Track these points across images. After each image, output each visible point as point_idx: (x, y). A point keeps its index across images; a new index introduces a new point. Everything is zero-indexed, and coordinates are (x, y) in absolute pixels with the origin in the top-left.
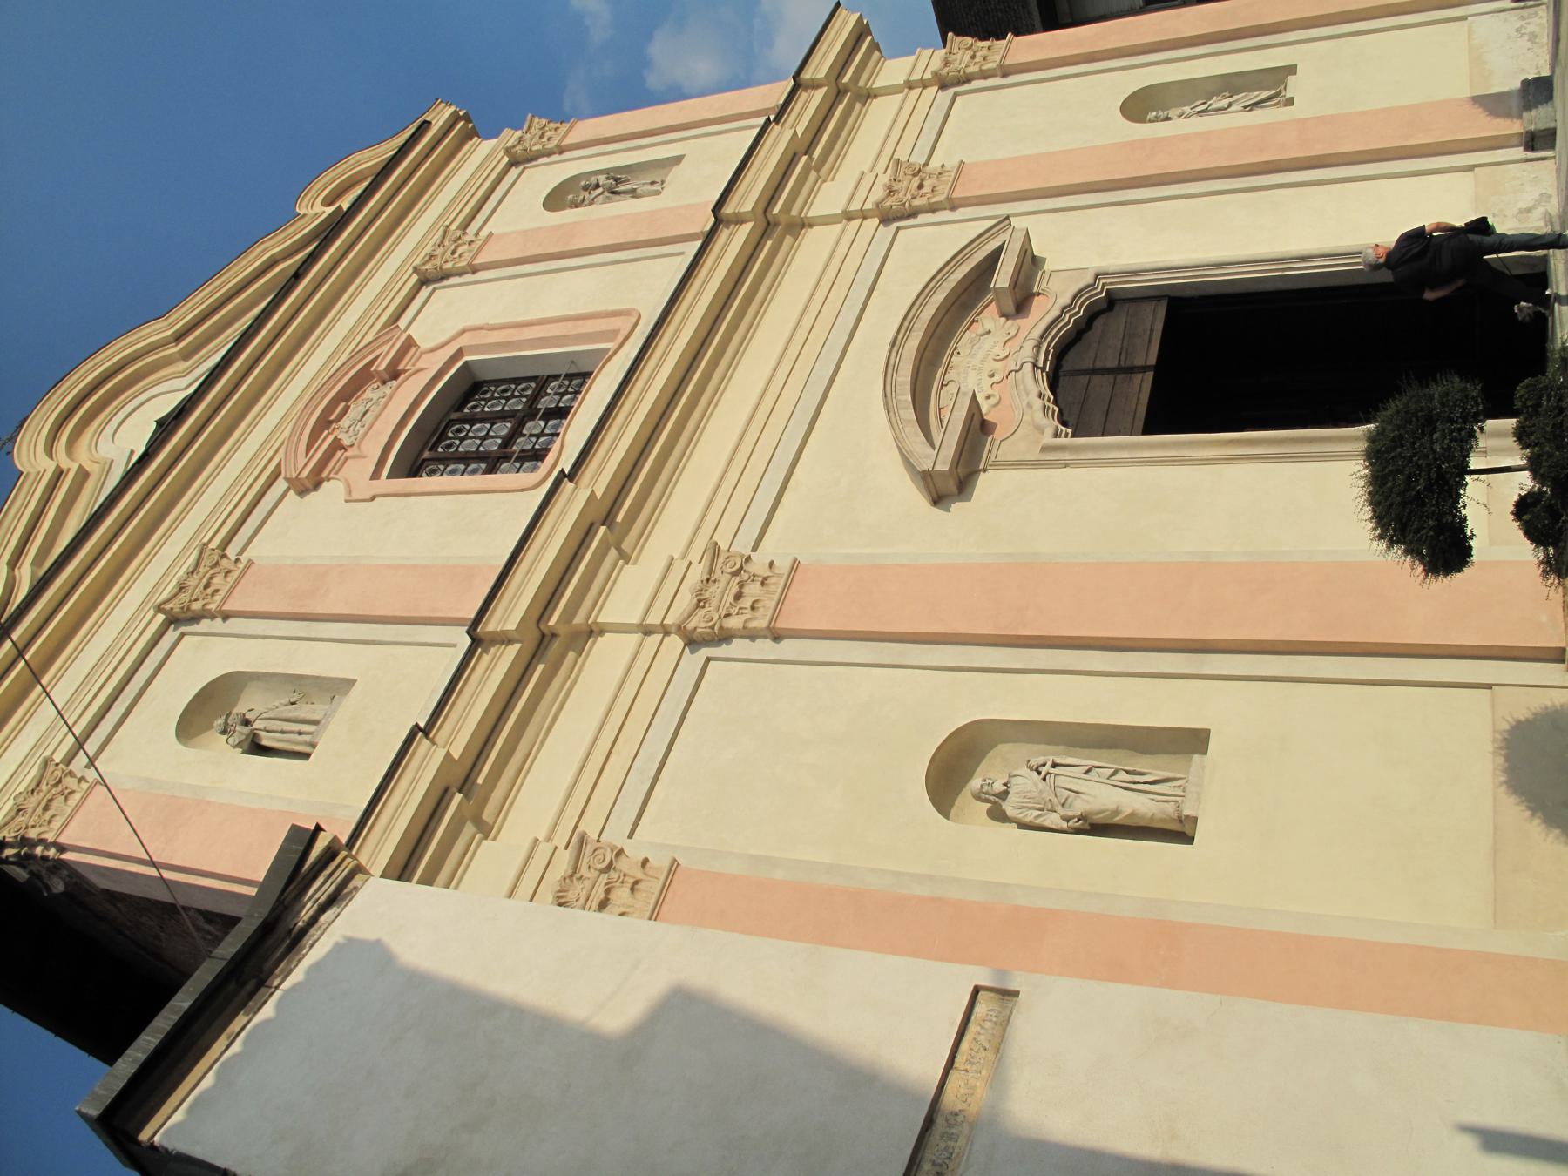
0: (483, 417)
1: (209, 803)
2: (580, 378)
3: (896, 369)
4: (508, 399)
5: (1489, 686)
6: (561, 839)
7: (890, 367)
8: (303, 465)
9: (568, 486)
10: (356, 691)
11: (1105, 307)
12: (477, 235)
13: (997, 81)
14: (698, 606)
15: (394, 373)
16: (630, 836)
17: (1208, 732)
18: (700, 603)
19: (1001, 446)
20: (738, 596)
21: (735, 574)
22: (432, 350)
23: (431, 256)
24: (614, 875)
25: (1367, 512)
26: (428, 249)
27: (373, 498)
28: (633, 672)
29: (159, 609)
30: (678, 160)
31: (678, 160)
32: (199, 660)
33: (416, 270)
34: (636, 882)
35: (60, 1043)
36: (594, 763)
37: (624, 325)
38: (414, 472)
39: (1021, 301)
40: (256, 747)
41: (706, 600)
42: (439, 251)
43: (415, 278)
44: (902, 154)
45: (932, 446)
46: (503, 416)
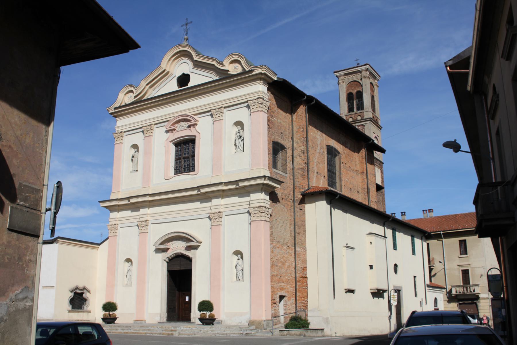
0: (185, 154)
19: (164, 254)
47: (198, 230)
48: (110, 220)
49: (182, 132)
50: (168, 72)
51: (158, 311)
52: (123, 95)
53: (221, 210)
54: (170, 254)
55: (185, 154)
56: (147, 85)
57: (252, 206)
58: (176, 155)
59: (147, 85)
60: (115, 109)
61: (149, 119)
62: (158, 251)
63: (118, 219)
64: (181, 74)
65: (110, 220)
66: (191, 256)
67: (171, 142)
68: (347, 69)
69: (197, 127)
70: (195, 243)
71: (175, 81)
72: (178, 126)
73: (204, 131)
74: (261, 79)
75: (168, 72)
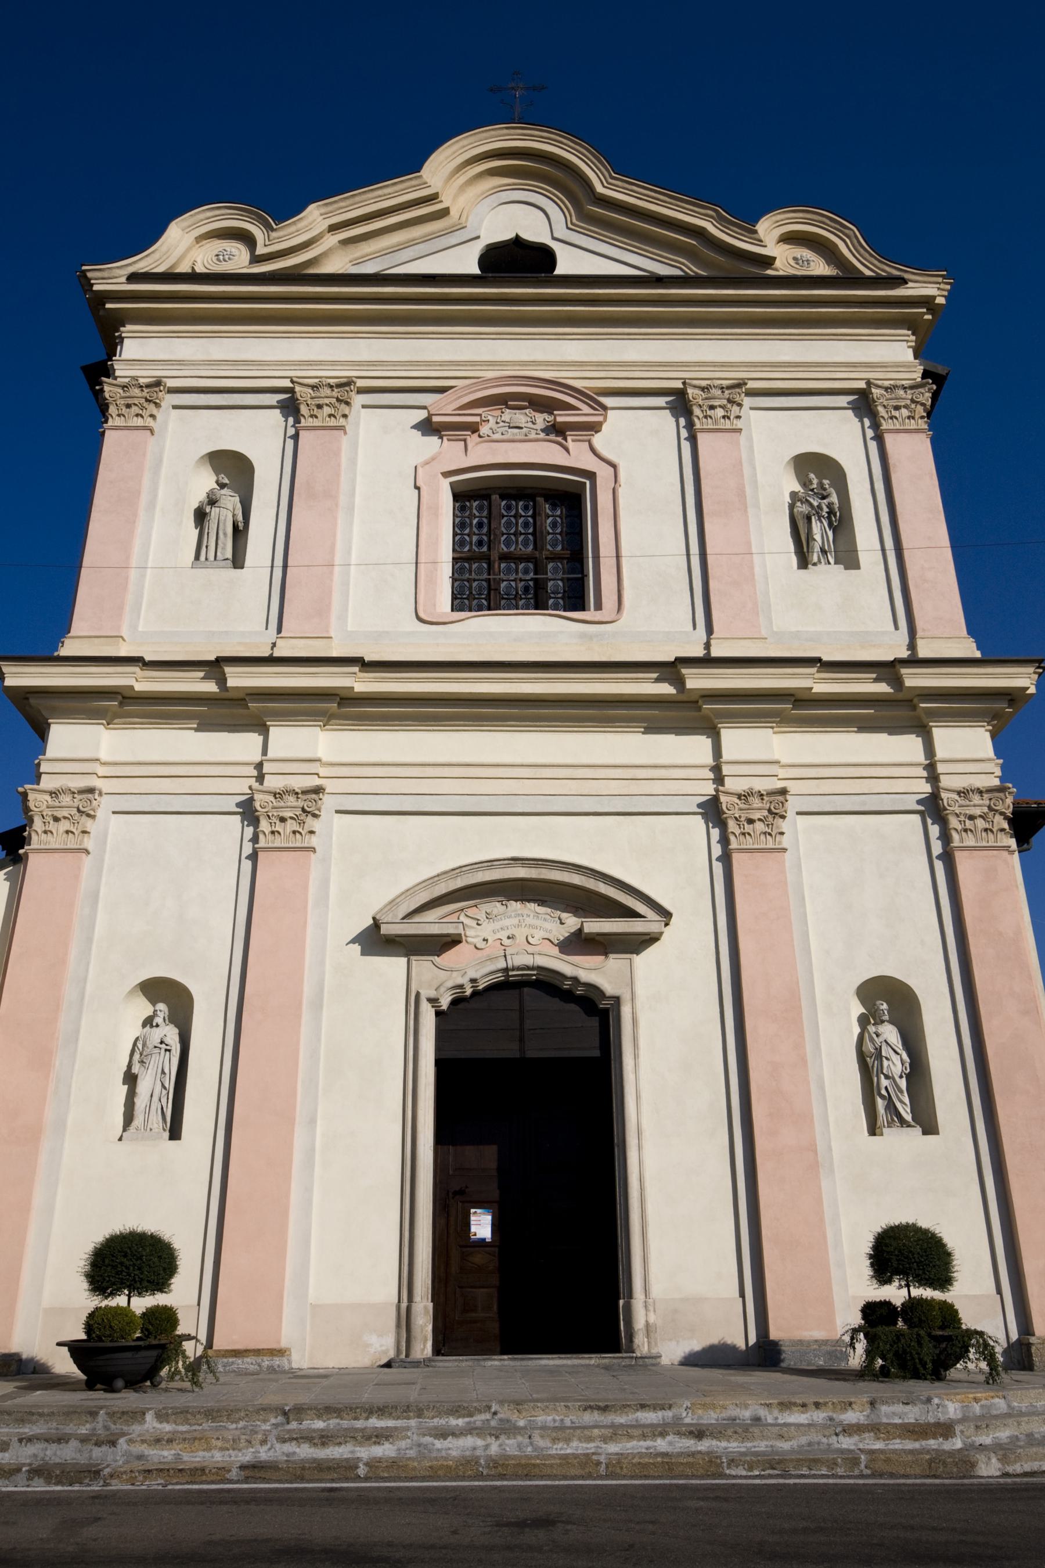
0: (527, 539)
3: (478, 870)
5: (199, 1304)
7: (491, 863)
8: (444, 408)
11: (600, 1014)
13: (937, 848)
14: (275, 794)
15: (558, 431)
16: (798, 813)
17: (937, 1133)
18: (963, 793)
19: (424, 967)
20: (972, 818)
21: (304, 810)
22: (593, 450)
24: (770, 818)
25: (139, 1230)
27: (417, 488)
28: (446, 769)
29: (869, 383)
32: (259, 435)
34: (72, 833)
36: (126, 770)
39: (579, 943)
41: (57, 797)
42: (717, 392)
45: (403, 918)
47: (663, 860)
48: (948, 287)
49: (517, 447)
50: (445, 212)
51: (385, 1290)
52: (192, 239)
53: (98, 783)
54: (469, 967)
55: (527, 539)
56: (333, 228)
57: (271, 782)
58: (458, 544)
59: (333, 228)
60: (133, 278)
61: (334, 363)
62: (376, 940)
63: (102, 771)
64: (507, 235)
65: (946, 293)
66: (609, 988)
67: (446, 474)
68: (688, 555)
69: (598, 440)
70: (650, 923)
71: (475, 250)
72: (492, 420)
73: (634, 459)
74: (911, 324)
75: (445, 212)
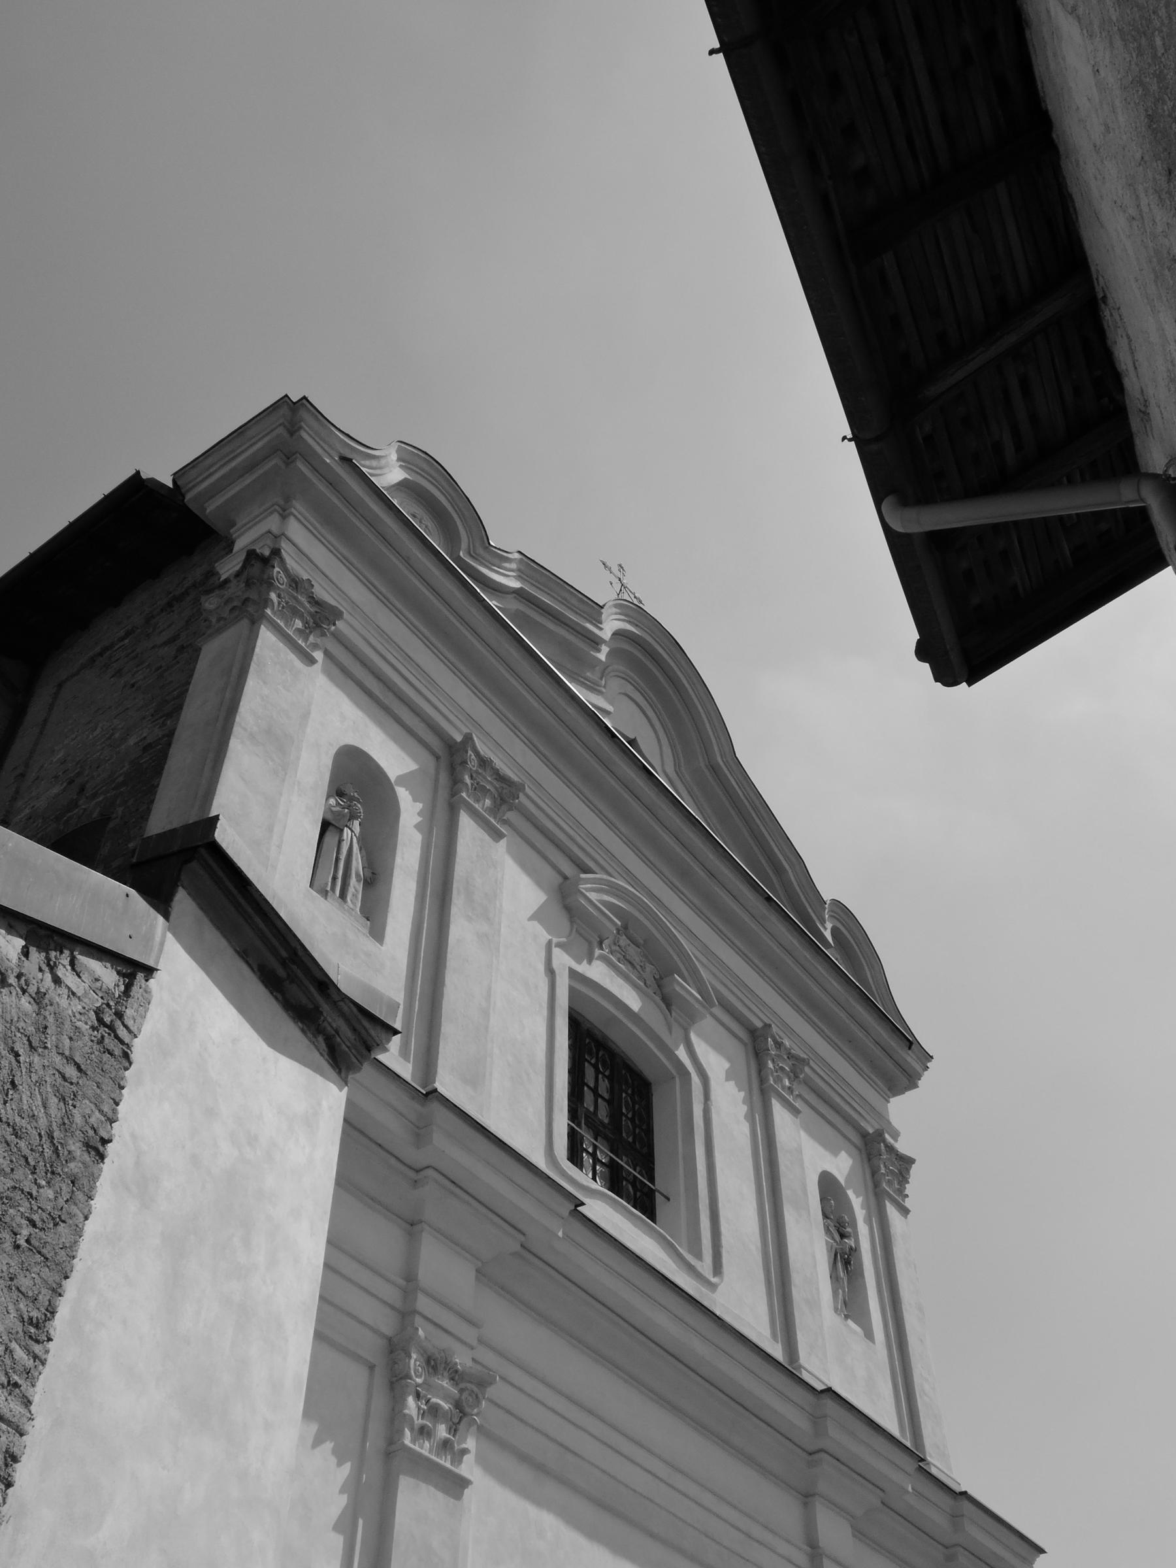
1: (284, 780)
2: (644, 1202)
4: (632, 1120)
6: (489, 1358)
9: (566, 1208)
10: (369, 944)
12: (799, 1096)
23: (779, 1045)
26: (787, 1043)
29: (468, 738)
30: (869, 1335)
31: (869, 1335)
33: (767, 1026)
35: (24, 555)
37: (705, 1266)
38: (576, 1024)
40: (326, 826)
43: (759, 1024)
44: (497, 1391)
46: (615, 1115)
